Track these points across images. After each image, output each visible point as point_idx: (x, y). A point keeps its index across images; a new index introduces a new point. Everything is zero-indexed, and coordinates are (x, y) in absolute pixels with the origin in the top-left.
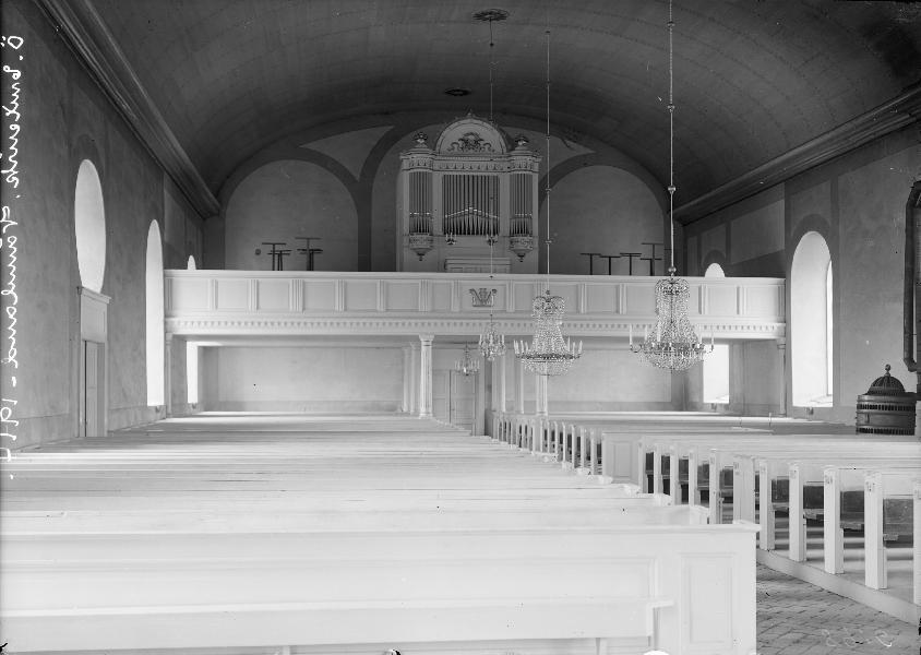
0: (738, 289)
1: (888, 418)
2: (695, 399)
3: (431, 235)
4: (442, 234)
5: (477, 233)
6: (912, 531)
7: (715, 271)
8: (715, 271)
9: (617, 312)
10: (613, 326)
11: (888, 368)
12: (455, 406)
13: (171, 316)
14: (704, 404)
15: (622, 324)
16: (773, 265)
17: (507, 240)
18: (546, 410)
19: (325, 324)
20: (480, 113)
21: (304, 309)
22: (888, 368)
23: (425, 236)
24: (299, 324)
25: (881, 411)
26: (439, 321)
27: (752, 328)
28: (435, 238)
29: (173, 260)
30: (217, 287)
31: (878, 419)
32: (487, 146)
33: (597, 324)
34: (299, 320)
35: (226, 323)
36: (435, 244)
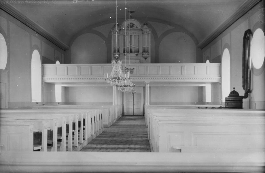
0: (206, 67)
1: (233, 103)
2: (204, 101)
3: (120, 53)
4: (123, 52)
5: (132, 52)
6: (48, 138)
7: (58, 62)
8: (58, 62)
9: (170, 74)
10: (142, 78)
11: (234, 88)
12: (135, 103)
13: (44, 77)
14: (206, 102)
15: (149, 78)
16: (217, 60)
17: (141, 54)
18: (149, 103)
19: (86, 79)
20: (135, 18)
21: (80, 74)
22: (234, 88)
23: (146, 53)
24: (86, 79)
25: (231, 102)
26: (138, 78)
27: (212, 79)
28: (121, 54)
29: (45, 60)
30: (56, 68)
31: (233, 104)
32: (136, 27)
33: (140, 78)
34: (98, 78)
35: (51, 79)
36: (121, 56)
